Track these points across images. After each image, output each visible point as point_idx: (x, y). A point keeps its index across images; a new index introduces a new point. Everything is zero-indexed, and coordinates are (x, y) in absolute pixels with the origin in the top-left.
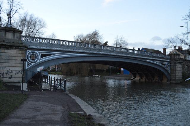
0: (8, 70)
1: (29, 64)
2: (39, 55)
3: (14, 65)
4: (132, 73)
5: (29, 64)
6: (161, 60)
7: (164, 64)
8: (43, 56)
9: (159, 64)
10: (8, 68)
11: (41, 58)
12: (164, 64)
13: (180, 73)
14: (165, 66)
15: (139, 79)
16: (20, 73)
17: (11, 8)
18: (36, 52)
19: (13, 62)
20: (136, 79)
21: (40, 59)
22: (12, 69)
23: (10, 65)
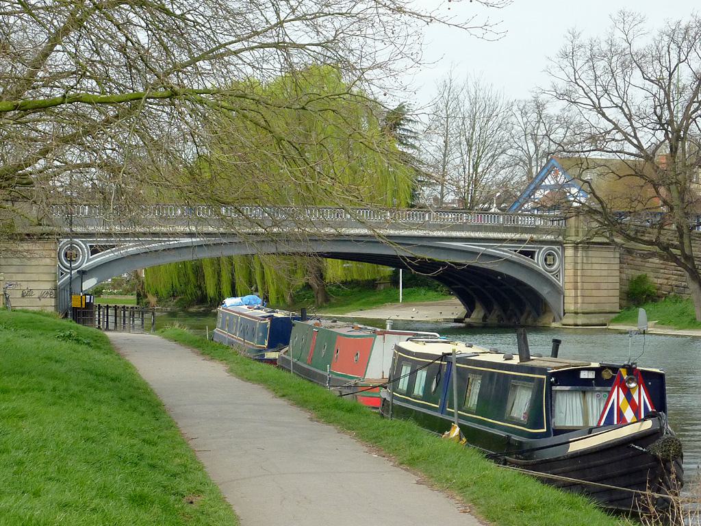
0: (24, 290)
1: (62, 274)
2: (84, 247)
3: (35, 277)
4: (454, 290)
5: (62, 274)
6: (518, 236)
7: (530, 254)
8: (94, 251)
9: (506, 253)
10: (24, 286)
11: (91, 257)
12: (530, 254)
13: (604, 286)
14: (538, 262)
15: (482, 314)
16: (49, 296)
17: (547, 92)
18: (555, 247)
19: (33, 270)
20: (474, 315)
21: (89, 260)
22: (32, 286)
23: (27, 277)
